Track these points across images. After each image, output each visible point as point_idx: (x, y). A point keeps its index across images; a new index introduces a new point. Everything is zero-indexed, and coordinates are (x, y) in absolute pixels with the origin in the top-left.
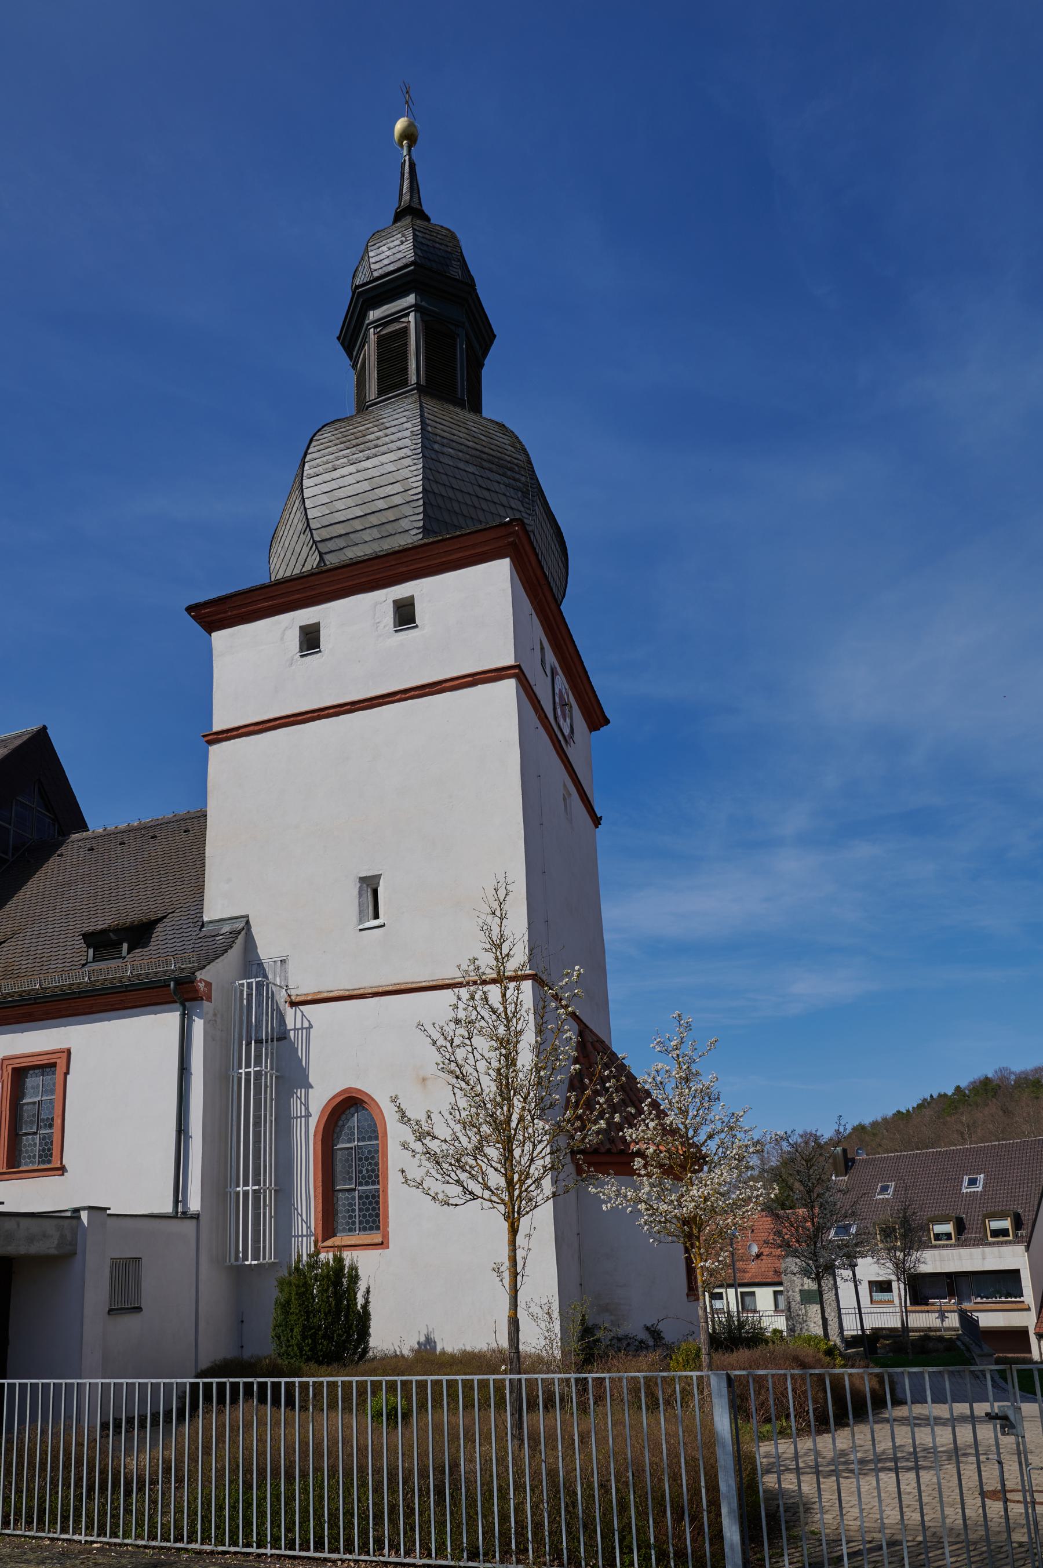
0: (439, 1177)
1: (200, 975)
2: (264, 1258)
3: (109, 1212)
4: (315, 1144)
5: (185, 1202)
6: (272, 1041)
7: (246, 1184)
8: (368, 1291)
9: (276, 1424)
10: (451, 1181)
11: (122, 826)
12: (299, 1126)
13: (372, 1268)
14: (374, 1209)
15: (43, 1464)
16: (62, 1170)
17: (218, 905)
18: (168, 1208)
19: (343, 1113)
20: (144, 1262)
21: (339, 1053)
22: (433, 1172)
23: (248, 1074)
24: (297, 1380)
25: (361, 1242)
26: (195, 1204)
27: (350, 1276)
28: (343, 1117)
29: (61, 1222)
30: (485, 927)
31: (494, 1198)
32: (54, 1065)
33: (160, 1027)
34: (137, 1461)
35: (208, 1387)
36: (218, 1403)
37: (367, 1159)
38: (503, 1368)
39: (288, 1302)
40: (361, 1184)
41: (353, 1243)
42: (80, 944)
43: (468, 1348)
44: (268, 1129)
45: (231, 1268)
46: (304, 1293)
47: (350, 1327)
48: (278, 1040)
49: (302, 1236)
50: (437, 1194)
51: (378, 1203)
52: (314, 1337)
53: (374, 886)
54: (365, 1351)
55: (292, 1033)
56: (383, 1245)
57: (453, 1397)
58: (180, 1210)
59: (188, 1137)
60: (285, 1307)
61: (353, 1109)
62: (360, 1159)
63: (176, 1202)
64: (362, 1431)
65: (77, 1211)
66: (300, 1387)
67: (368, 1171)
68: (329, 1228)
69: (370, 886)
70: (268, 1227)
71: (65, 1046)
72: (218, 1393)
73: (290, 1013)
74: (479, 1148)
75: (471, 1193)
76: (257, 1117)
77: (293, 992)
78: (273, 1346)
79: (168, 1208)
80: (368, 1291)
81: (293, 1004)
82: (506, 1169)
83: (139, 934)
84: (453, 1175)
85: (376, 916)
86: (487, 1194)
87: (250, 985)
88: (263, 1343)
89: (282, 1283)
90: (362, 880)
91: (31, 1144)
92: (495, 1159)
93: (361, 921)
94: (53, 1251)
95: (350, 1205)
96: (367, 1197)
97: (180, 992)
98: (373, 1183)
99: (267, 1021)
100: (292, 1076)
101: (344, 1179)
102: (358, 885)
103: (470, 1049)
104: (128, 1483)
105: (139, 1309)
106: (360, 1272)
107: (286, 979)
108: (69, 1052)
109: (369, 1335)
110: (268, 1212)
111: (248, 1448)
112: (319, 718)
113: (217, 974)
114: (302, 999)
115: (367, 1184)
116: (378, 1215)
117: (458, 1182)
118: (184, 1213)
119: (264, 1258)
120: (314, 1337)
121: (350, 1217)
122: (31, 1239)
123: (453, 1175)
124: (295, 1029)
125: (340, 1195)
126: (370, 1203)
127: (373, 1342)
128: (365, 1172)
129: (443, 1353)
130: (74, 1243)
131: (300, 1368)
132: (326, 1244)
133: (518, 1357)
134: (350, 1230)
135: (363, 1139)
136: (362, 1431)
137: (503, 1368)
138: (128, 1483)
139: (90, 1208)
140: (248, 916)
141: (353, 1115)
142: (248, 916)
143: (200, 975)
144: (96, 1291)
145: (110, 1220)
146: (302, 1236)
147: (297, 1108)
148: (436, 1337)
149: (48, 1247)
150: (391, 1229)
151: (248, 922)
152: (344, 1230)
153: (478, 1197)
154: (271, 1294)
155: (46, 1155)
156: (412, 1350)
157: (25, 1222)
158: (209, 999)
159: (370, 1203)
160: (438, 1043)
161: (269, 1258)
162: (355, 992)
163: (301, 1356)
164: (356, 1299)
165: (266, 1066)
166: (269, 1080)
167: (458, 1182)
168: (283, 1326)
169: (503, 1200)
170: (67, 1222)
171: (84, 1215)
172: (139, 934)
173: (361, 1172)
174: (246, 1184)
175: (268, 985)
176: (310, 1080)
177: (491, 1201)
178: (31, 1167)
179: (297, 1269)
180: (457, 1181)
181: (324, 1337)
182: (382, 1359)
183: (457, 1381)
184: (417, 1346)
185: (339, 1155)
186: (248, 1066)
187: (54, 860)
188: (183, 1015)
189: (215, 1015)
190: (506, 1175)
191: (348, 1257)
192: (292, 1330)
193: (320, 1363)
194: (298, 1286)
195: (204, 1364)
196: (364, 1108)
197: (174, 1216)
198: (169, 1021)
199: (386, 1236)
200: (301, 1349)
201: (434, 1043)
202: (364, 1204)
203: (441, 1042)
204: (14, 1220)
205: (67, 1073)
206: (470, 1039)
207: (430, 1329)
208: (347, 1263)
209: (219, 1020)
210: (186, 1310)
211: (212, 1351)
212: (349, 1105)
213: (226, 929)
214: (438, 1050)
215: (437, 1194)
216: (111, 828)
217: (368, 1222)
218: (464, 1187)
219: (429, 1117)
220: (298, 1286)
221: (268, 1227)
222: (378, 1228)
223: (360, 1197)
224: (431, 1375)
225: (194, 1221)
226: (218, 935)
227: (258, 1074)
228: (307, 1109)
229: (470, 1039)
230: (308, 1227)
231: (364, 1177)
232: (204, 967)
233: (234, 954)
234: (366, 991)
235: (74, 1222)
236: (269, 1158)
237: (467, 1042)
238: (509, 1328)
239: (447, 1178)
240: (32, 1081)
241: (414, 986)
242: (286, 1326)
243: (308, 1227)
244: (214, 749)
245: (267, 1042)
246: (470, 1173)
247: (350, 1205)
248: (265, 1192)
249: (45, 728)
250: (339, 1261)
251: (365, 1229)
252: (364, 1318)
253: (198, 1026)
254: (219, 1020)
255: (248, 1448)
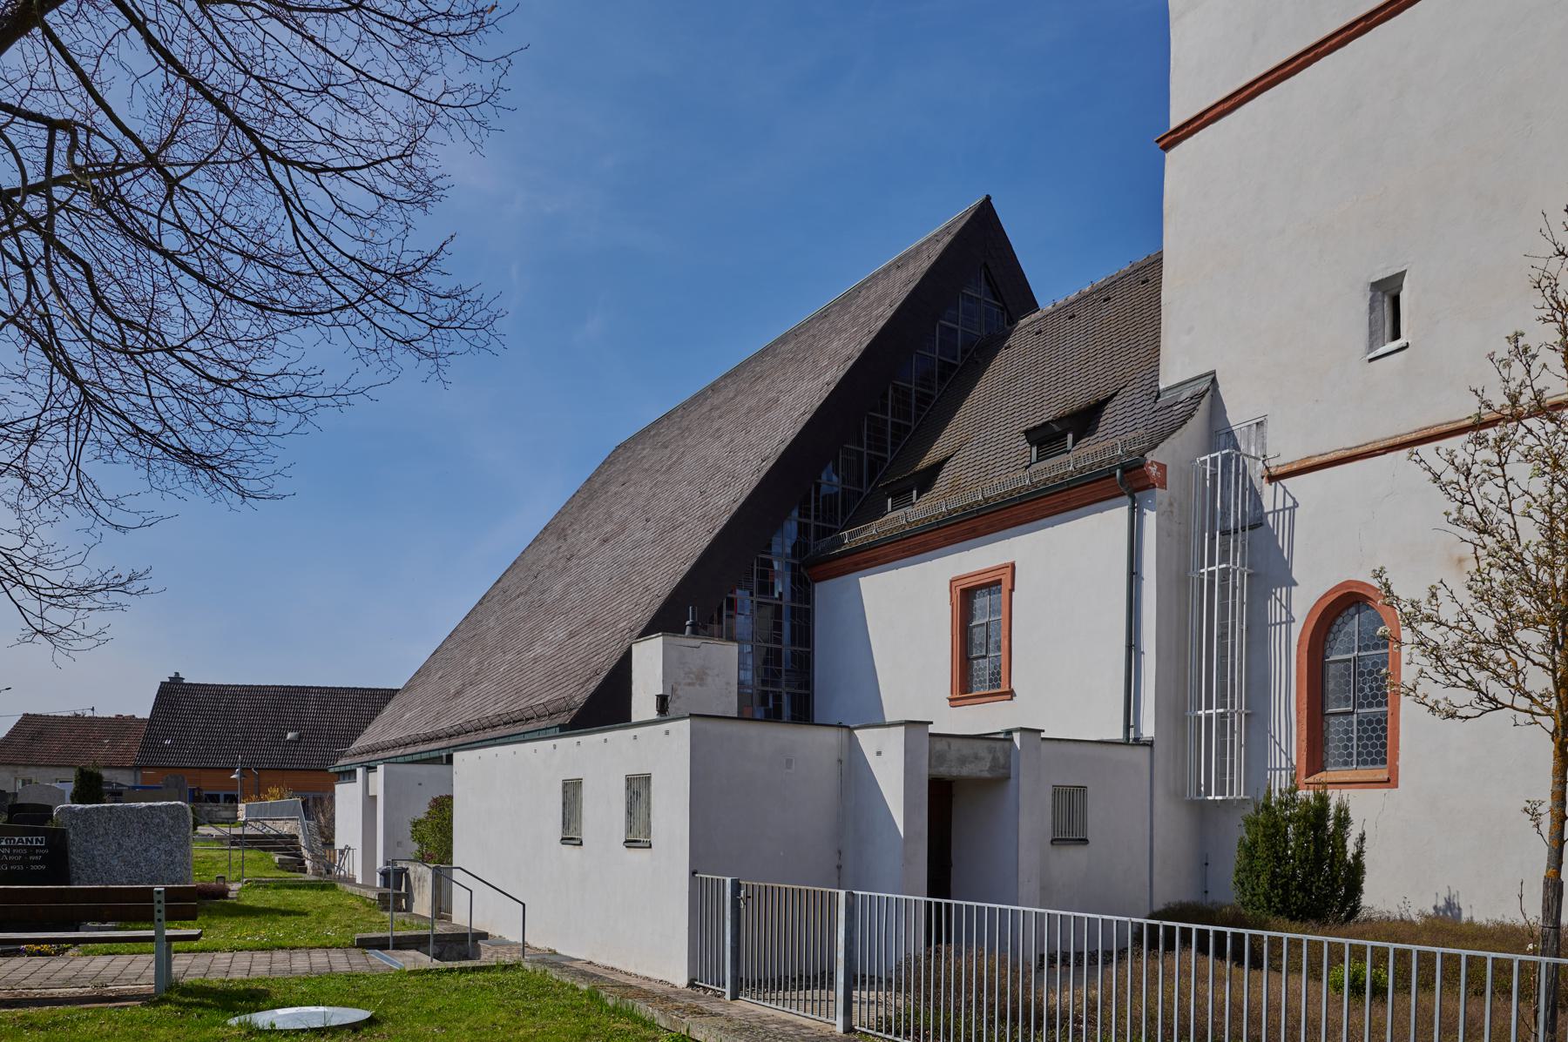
0: (1441, 678)
1: (1150, 457)
2: (1231, 793)
3: (1043, 735)
4: (1298, 656)
5: (1137, 730)
6: (1243, 529)
7: (1209, 706)
8: (1362, 839)
9: (1201, 978)
10: (1460, 683)
11: (1073, 296)
12: (1277, 637)
13: (1371, 816)
14: (1379, 737)
15: (948, 985)
16: (1011, 694)
17: (1177, 367)
18: (1119, 735)
19: (1339, 615)
20: (1089, 790)
21: (1338, 534)
22: (1430, 671)
23: (1212, 574)
24: (1266, 934)
25: (1358, 779)
26: (1148, 730)
27: (1337, 818)
28: (1339, 621)
29: (993, 744)
30: (1544, 283)
31: (1536, 709)
32: (999, 582)
33: (1106, 526)
34: (1062, 996)
35: (1170, 931)
36: (1149, 949)
37: (1370, 673)
38: (1531, 946)
39: (1254, 843)
40: (1361, 706)
41: (1347, 779)
42: (1023, 442)
43: (1507, 921)
44: (1239, 640)
45: (1192, 802)
46: (1273, 836)
47: (1335, 879)
48: (1251, 528)
49: (1281, 769)
50: (1437, 702)
51: (1384, 729)
52: (1285, 887)
53: (1394, 292)
54: (1355, 911)
55: (1270, 517)
56: (1390, 782)
57: (1451, 977)
58: (1132, 736)
59: (1140, 653)
60: (1249, 850)
61: (1352, 610)
62: (1361, 674)
63: (1127, 727)
64: (1313, 1002)
65: (1009, 732)
66: (1469, 964)
67: (1371, 689)
68: (1316, 758)
69: (1388, 293)
70: (1239, 757)
71: (1009, 561)
72: (1216, 943)
73: (1268, 492)
74: (1505, 633)
75: (1492, 700)
76: (1223, 626)
77: (1272, 463)
78: (1236, 894)
79: (1119, 735)
80: (1362, 839)
81: (1272, 479)
82: (1553, 661)
83: (1084, 420)
84: (1462, 674)
85: (1396, 335)
86: (1522, 703)
87: (1214, 460)
88: (1227, 893)
89: (1251, 823)
90: (1376, 286)
91: (982, 667)
92: (1534, 646)
93: (1372, 347)
94: (986, 774)
95: (1346, 732)
96: (1370, 722)
97: (1128, 481)
98: (1379, 704)
99: (1236, 505)
100: (1270, 571)
101: (1338, 700)
102: (1369, 295)
103: (1501, 481)
104: (1051, 1018)
105: (1085, 841)
106: (1352, 815)
107: (1264, 446)
108: (1013, 566)
109: (1361, 891)
110: (1239, 738)
111: (1168, 1002)
112: (1317, 58)
113: (1177, 454)
114: (1284, 470)
115: (1370, 705)
116: (1384, 745)
117: (1471, 684)
118: (1136, 739)
119: (1231, 793)
120: (1285, 887)
121: (1346, 747)
122: (963, 761)
123: (1462, 674)
124: (1274, 511)
125: (1332, 720)
126: (1374, 730)
127: (1366, 900)
128: (1367, 690)
129: (1470, 922)
130: (1007, 767)
131: (1267, 921)
132: (1311, 779)
133: (1557, 936)
134: (1346, 763)
135: (1367, 648)
136: (1313, 1002)
137: (1531, 946)
138: (1051, 1018)
139: (1022, 730)
140: (1214, 372)
141: (1353, 617)
142: (1214, 372)
143: (1150, 457)
144: (1032, 815)
145: (1044, 745)
146: (1281, 769)
147: (1276, 612)
148: (1462, 902)
149: (980, 769)
150: (1401, 762)
151: (1214, 381)
152: (1336, 764)
153: (1504, 706)
154: (1235, 833)
155: (995, 679)
156: (1421, 914)
157: (955, 743)
158: (1163, 485)
159: (1374, 730)
160: (1444, 478)
161: (1239, 794)
162: (1360, 450)
163: (1269, 908)
164: (1344, 847)
165: (1236, 563)
166: (1240, 580)
167: (1471, 684)
168: (1248, 871)
169: (1549, 710)
170: (999, 744)
171: (1016, 737)
172: (1084, 420)
173: (1361, 690)
174: (1209, 706)
175: (1237, 457)
176: (1294, 575)
177: (1533, 713)
178: (982, 692)
179: (1267, 807)
180: (1468, 683)
181: (1300, 887)
182: (1380, 920)
183: (1343, 945)
184: (1431, 912)
185: (1332, 670)
186: (1211, 563)
187: (1003, 352)
188: (1132, 509)
189: (1171, 504)
190: (1554, 672)
191: (1334, 797)
192: (1258, 877)
193: (1293, 918)
194: (1265, 827)
195: (1159, 906)
196: (1369, 607)
197: (1126, 743)
198: (1115, 517)
199: (1394, 772)
200: (1269, 901)
201: (1437, 478)
202: (1365, 731)
203: (1450, 475)
204: (944, 741)
205: (1012, 590)
206: (1501, 465)
207: (1453, 892)
208: (1333, 803)
209: (1176, 511)
210: (1142, 849)
211: (1166, 895)
212: (1347, 603)
213: (1187, 394)
214: (1443, 487)
215: (1437, 702)
216: (1060, 302)
217: (1370, 754)
218: (1480, 691)
219: (1434, 595)
220: (1265, 827)
221: (1239, 757)
222: (1384, 761)
223: (1360, 723)
224: (1269, 929)
225: (1147, 749)
226: (1176, 404)
227: (1224, 572)
228: (1289, 612)
229: (1501, 465)
230: (1289, 759)
231: (1365, 697)
232: (1156, 446)
233: (1196, 425)
234: (1376, 446)
235: (1007, 744)
236: (1239, 676)
237: (1498, 471)
238: (1545, 893)
239: (1454, 679)
240: (981, 602)
241: (1451, 427)
242: (1251, 871)
243: (1289, 759)
244: (1172, 156)
245: (1236, 532)
246: (1494, 672)
247: (1346, 732)
248: (1232, 715)
249: (988, 198)
250: (1323, 800)
251: (1365, 763)
252: (1355, 872)
253: (1150, 519)
254: (1176, 511)
255: (1168, 1002)
